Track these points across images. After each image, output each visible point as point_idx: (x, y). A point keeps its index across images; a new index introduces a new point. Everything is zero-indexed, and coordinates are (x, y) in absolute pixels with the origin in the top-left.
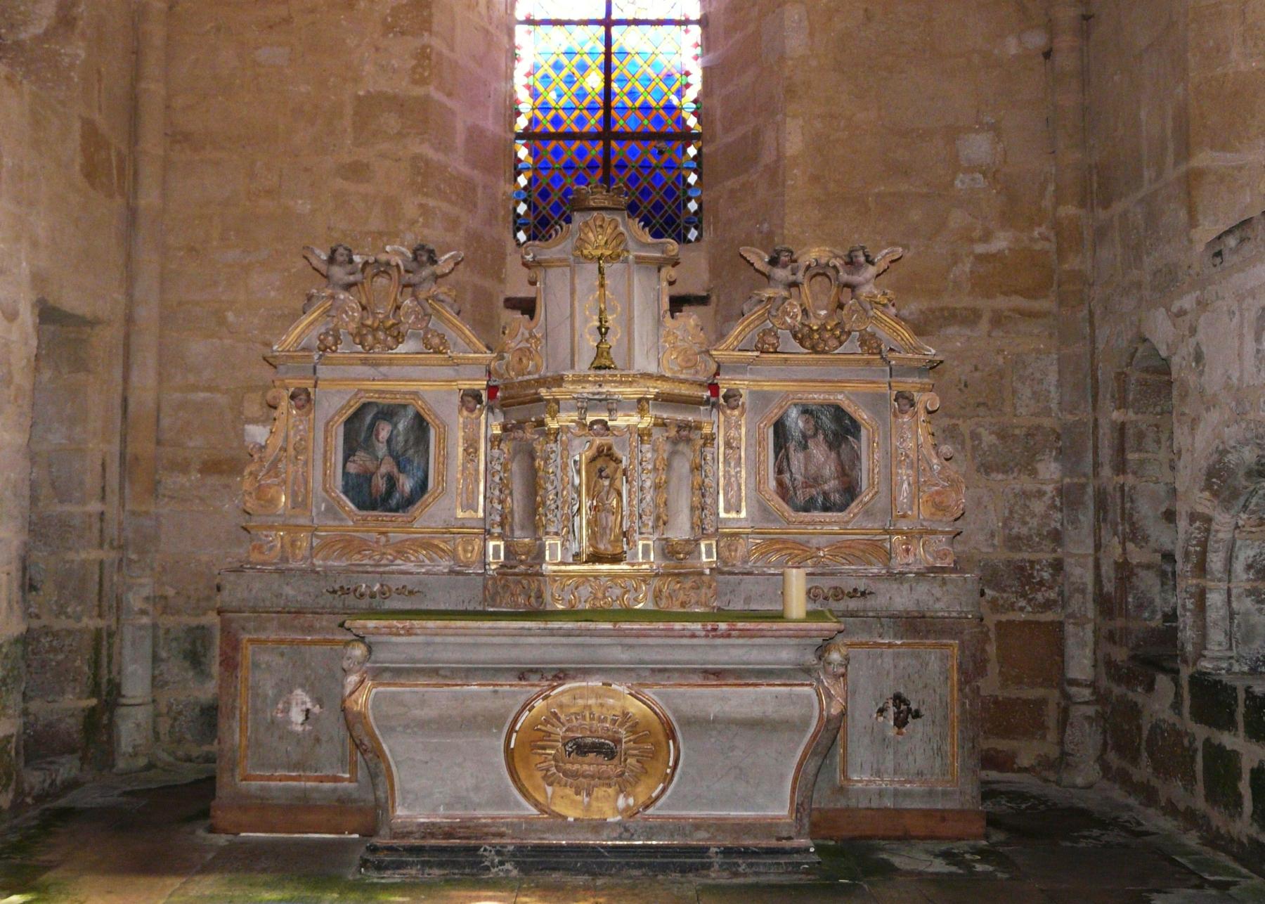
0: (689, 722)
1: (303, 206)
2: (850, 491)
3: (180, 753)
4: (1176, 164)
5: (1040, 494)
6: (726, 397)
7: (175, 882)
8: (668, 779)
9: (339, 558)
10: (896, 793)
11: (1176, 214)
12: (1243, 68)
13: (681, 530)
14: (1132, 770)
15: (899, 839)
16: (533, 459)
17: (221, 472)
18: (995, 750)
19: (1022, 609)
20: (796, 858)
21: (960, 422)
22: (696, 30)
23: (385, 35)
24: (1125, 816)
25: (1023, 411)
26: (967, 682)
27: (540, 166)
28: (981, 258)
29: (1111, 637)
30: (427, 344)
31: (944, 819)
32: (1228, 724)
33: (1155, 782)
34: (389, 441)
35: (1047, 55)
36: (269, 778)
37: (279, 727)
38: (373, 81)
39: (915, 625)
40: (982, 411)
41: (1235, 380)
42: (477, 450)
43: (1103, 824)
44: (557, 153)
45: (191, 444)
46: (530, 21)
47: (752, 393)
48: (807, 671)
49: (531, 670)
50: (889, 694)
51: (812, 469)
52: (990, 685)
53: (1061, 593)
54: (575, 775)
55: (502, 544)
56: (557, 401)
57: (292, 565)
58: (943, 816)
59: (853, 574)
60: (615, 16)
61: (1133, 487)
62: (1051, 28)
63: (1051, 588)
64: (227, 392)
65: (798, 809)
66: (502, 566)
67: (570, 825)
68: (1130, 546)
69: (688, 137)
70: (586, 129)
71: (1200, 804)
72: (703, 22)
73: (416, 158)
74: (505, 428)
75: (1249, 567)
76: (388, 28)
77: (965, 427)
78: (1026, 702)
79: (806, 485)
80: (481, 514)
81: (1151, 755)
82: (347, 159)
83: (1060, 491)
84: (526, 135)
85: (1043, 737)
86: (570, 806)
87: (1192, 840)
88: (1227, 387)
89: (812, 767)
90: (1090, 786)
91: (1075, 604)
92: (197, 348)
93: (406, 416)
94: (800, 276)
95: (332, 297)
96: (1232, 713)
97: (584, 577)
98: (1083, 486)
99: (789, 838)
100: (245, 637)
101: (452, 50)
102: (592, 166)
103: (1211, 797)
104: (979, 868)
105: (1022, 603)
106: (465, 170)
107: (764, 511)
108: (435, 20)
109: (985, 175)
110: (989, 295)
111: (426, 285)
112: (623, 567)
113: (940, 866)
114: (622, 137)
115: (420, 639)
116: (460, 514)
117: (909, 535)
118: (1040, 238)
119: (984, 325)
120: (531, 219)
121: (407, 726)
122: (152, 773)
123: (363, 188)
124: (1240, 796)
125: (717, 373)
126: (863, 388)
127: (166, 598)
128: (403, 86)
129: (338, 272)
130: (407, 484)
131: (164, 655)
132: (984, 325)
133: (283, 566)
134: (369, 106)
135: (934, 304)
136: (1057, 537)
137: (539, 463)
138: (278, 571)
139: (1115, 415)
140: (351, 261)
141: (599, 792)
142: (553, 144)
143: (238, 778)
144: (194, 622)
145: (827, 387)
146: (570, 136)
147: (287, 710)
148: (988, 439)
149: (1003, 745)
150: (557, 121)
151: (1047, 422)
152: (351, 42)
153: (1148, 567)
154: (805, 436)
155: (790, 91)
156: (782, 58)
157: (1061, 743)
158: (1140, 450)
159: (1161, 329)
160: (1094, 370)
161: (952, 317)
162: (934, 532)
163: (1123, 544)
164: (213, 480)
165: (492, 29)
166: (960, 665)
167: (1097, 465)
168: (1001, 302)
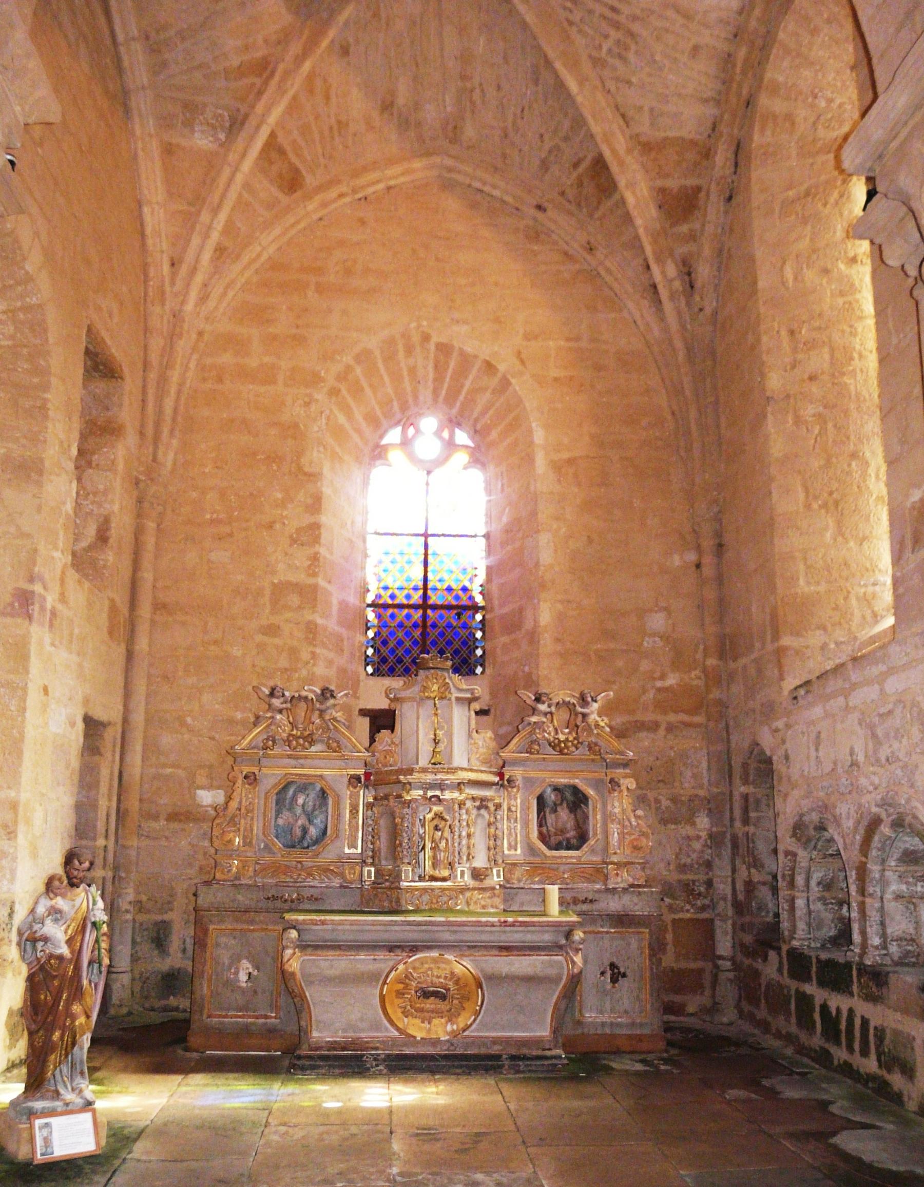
0: (490, 978)
1: (237, 652)
2: (583, 838)
3: (147, 1005)
4: (772, 642)
5: (698, 837)
6: (509, 781)
7: (178, 1078)
8: (477, 1014)
9: (272, 877)
10: (612, 1024)
11: (771, 672)
12: (806, 589)
13: (480, 862)
14: (756, 1012)
15: (615, 1053)
16: (394, 818)
17: (180, 821)
18: (673, 1002)
19: (688, 911)
20: (554, 1061)
21: (648, 793)
22: (483, 541)
23: (291, 545)
24: (751, 1040)
25: (686, 785)
26: (654, 955)
27: (383, 625)
28: (659, 690)
29: (743, 928)
30: (329, 747)
31: (641, 1040)
32: (807, 979)
33: (770, 1019)
34: (303, 806)
35: (698, 566)
36: (226, 1016)
37: (231, 985)
38: (283, 574)
39: (622, 920)
40: (661, 785)
41: (806, 773)
42: (357, 812)
43: (737, 1044)
44: (393, 616)
45: (162, 802)
46: (377, 533)
47: (524, 778)
48: (561, 947)
49: (399, 947)
50: (607, 963)
51: (560, 825)
52: (669, 960)
53: (712, 900)
54: (421, 1010)
55: (373, 869)
56: (410, 783)
57: (243, 882)
58: (640, 1038)
59: (584, 888)
60: (430, 532)
61: (754, 834)
62: (699, 548)
63: (705, 897)
64: (184, 769)
65: (555, 1031)
66: (374, 883)
67: (418, 1042)
68: (753, 870)
69: (476, 608)
70: (411, 602)
71: (794, 1029)
72: (487, 536)
73: (309, 623)
74: (375, 799)
75: (819, 884)
76: (293, 541)
77: (651, 795)
78: (693, 970)
79: (556, 834)
80: (359, 851)
81: (767, 1002)
82: (264, 622)
83: (711, 836)
84: (373, 605)
85: (702, 994)
86: (417, 1029)
87: (789, 1051)
88: (802, 776)
89: (563, 1006)
90: (731, 1024)
91: (721, 905)
92: (167, 740)
93: (314, 789)
94: (553, 709)
95: (272, 717)
96: (809, 973)
97: (425, 890)
98: (725, 833)
99: (550, 1049)
100: (211, 927)
101: (331, 554)
102: (415, 625)
103: (799, 1024)
104: (662, 1067)
105: (688, 907)
106: (337, 629)
107: (531, 850)
108: (323, 536)
109: (661, 638)
110: (665, 713)
111: (329, 711)
112: (448, 883)
113: (639, 1067)
114: (434, 607)
115: (330, 927)
116: (347, 851)
117: (619, 865)
118: (695, 678)
119: (662, 732)
120: (376, 659)
121: (321, 981)
122: (130, 1018)
123: (277, 641)
124: (814, 1023)
125: (503, 766)
126: (590, 775)
127: (141, 902)
128: (300, 577)
129: (276, 702)
130: (313, 832)
131: (138, 940)
132: (662, 732)
133: (237, 882)
134: (280, 590)
135: (631, 718)
136: (709, 865)
137: (398, 820)
138: (233, 885)
139: (743, 789)
140: (283, 695)
141: (436, 1021)
142: (390, 611)
143: (205, 1016)
144: (159, 918)
145: (570, 775)
146: (401, 606)
147: (236, 973)
148: (665, 803)
149: (678, 999)
150: (393, 597)
151: (702, 793)
152: (270, 549)
153: (764, 884)
154: (555, 804)
155: (543, 586)
156: (537, 564)
157: (713, 996)
158: (757, 811)
159: (767, 740)
160: (729, 759)
161: (641, 726)
162: (632, 863)
163: (748, 869)
164: (175, 825)
165: (354, 539)
166: (650, 944)
167: (732, 820)
168: (672, 718)
